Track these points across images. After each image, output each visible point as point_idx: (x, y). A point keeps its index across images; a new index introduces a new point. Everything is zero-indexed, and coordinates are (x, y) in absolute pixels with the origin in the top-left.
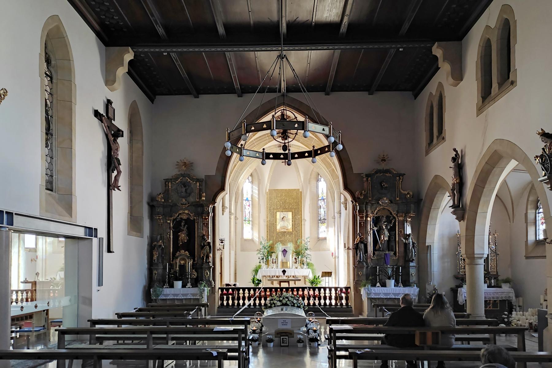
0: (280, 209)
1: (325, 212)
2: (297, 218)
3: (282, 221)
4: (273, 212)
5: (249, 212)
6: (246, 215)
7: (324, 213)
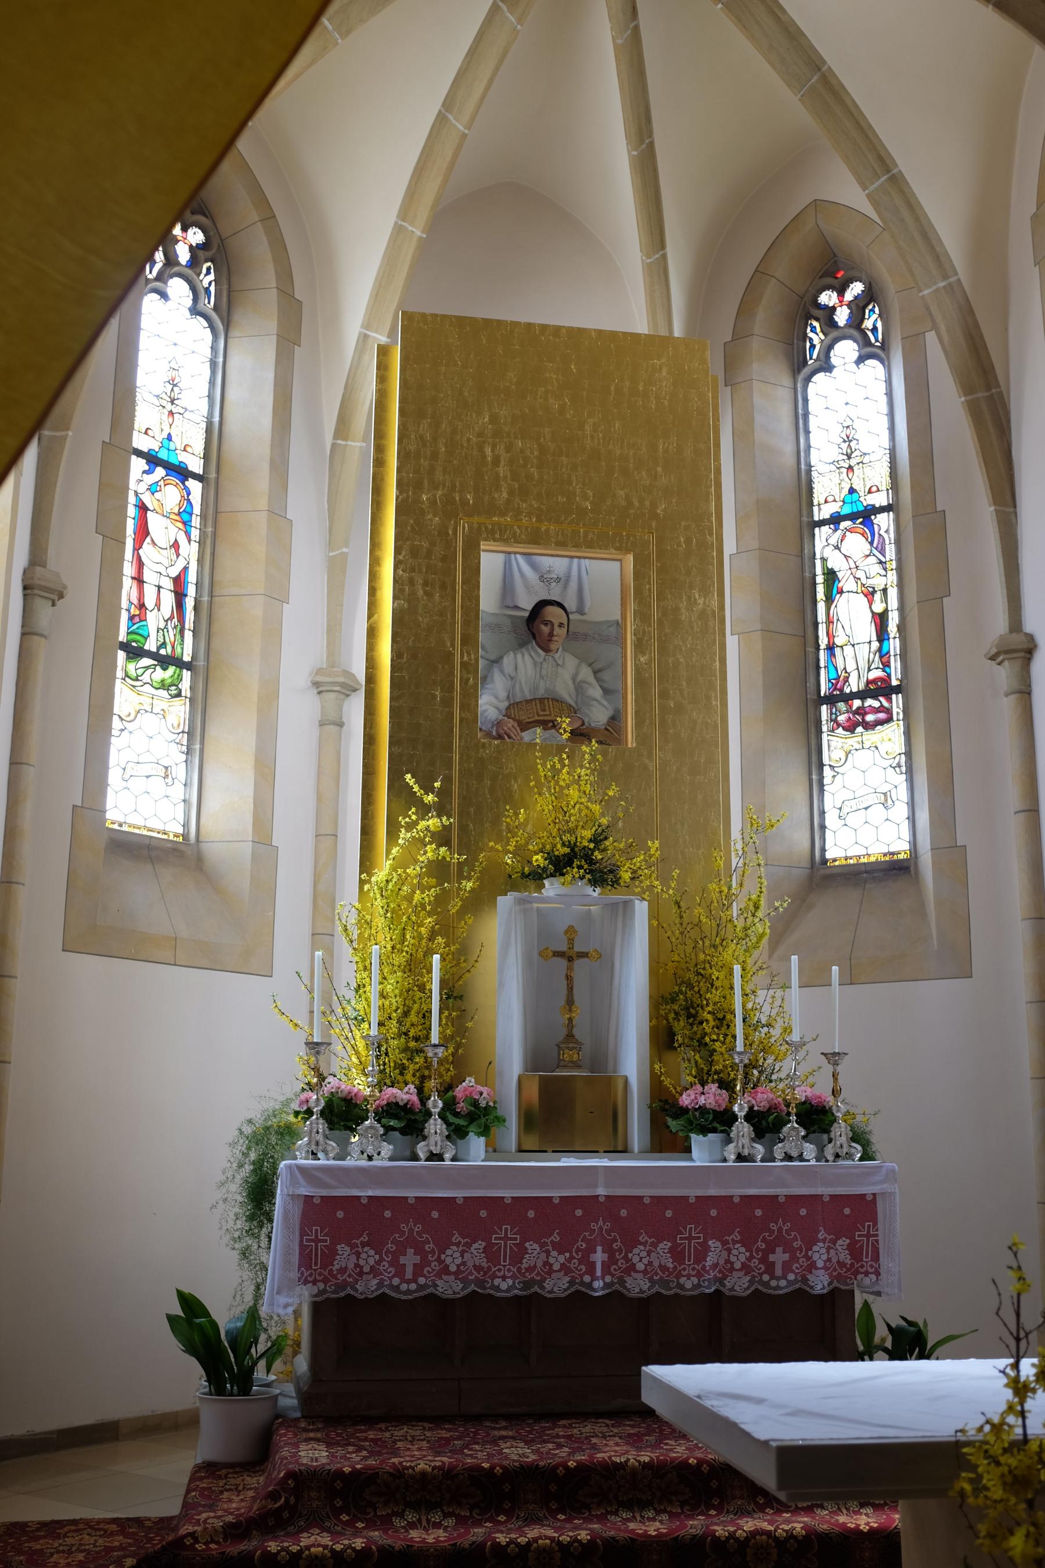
0: (518, 512)
1: (880, 620)
2: (684, 615)
3: (522, 645)
4: (443, 532)
5: (179, 582)
6: (150, 601)
7: (866, 631)
